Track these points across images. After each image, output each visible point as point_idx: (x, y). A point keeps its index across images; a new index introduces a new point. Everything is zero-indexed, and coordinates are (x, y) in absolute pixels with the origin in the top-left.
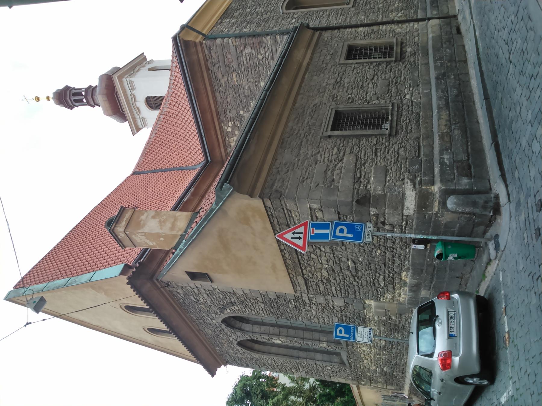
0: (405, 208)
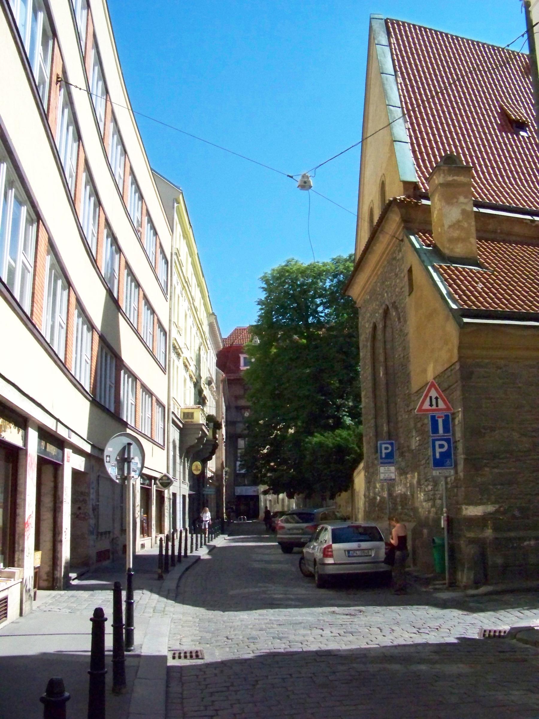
0: (467, 507)
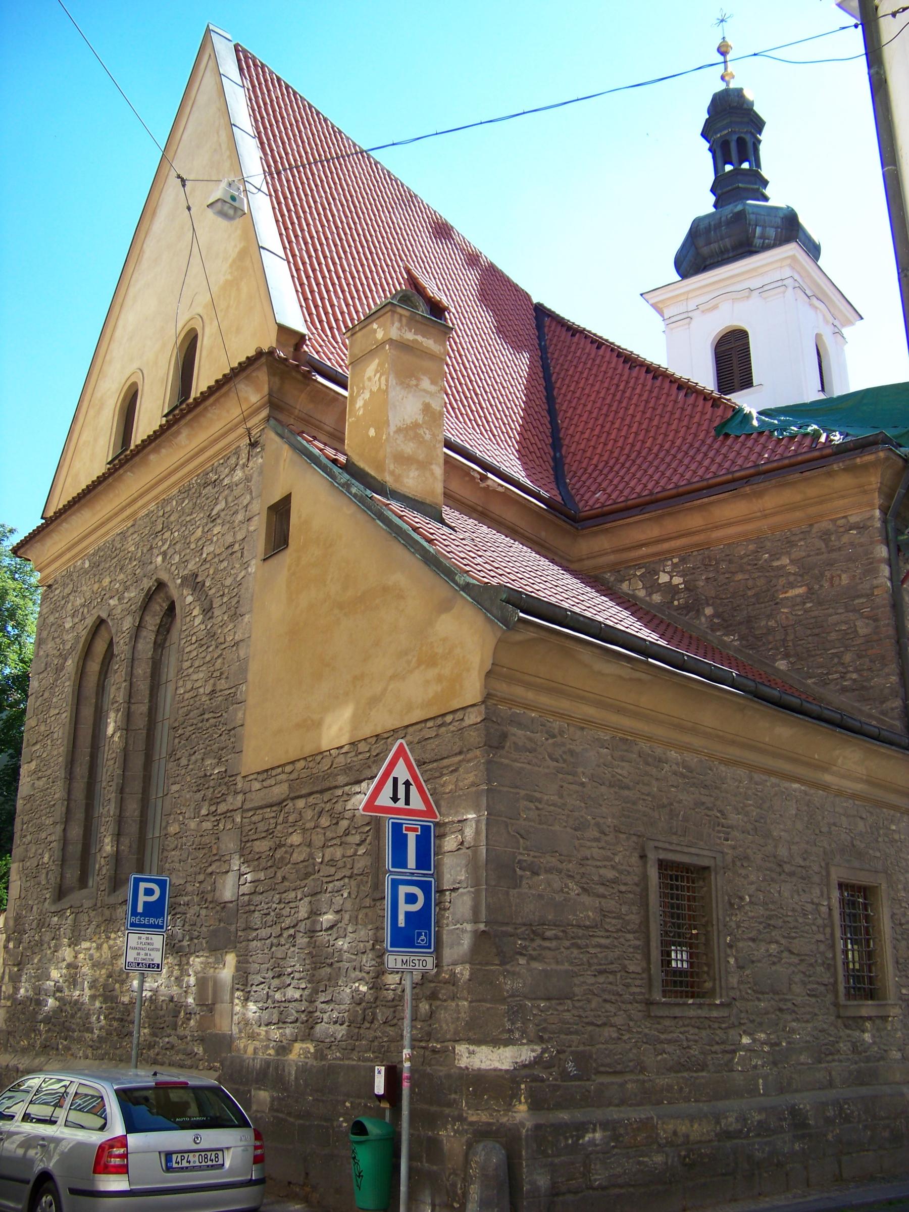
0: (471, 1048)
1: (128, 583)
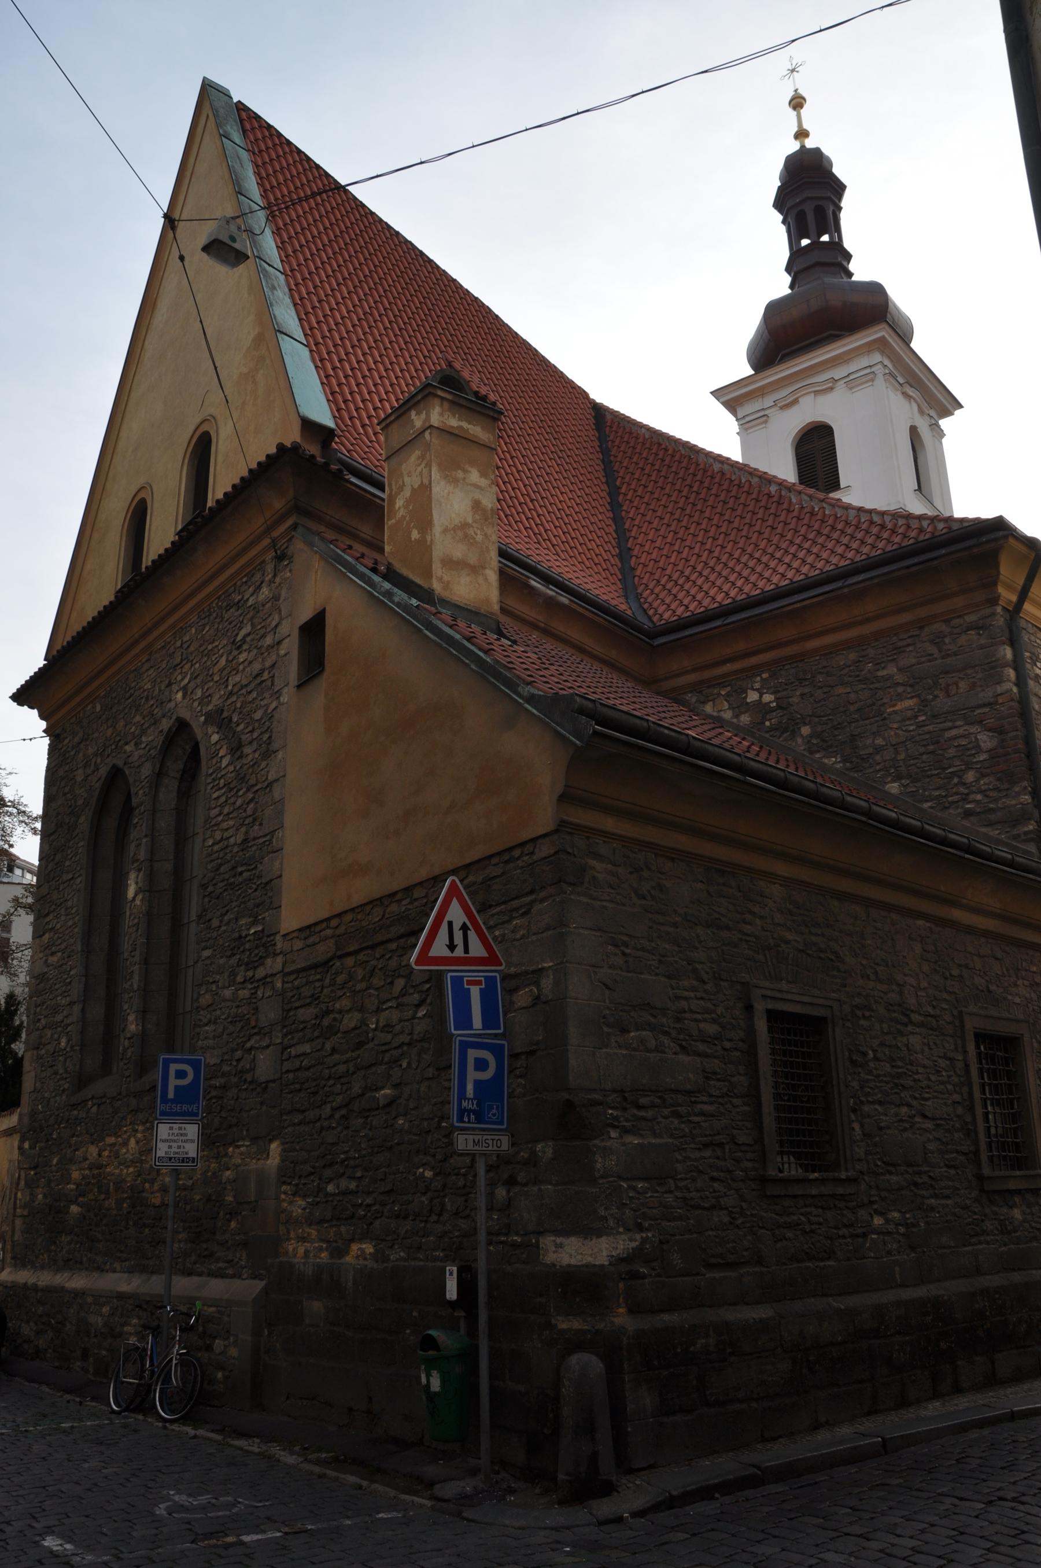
0: (559, 1240)
1: (146, 725)
